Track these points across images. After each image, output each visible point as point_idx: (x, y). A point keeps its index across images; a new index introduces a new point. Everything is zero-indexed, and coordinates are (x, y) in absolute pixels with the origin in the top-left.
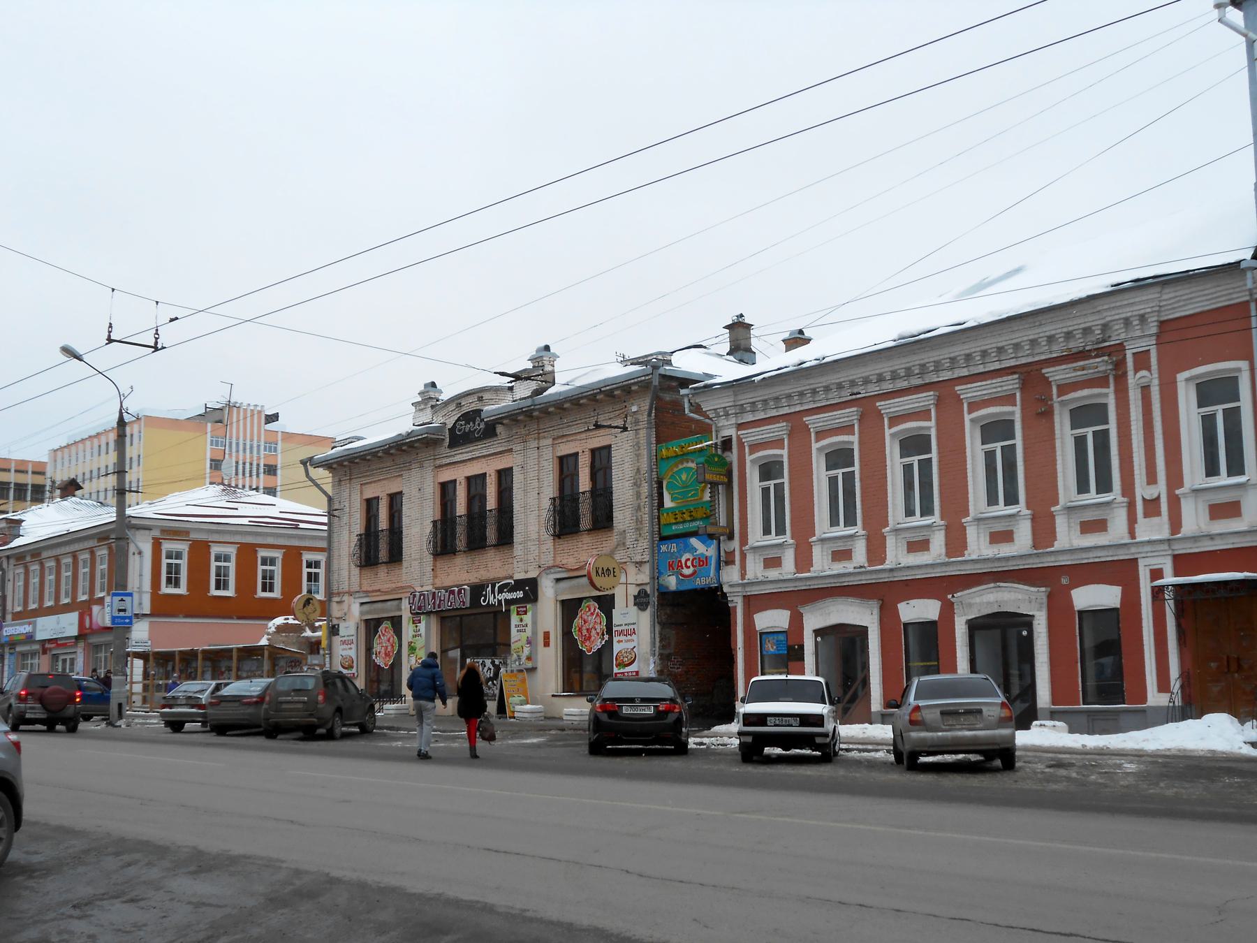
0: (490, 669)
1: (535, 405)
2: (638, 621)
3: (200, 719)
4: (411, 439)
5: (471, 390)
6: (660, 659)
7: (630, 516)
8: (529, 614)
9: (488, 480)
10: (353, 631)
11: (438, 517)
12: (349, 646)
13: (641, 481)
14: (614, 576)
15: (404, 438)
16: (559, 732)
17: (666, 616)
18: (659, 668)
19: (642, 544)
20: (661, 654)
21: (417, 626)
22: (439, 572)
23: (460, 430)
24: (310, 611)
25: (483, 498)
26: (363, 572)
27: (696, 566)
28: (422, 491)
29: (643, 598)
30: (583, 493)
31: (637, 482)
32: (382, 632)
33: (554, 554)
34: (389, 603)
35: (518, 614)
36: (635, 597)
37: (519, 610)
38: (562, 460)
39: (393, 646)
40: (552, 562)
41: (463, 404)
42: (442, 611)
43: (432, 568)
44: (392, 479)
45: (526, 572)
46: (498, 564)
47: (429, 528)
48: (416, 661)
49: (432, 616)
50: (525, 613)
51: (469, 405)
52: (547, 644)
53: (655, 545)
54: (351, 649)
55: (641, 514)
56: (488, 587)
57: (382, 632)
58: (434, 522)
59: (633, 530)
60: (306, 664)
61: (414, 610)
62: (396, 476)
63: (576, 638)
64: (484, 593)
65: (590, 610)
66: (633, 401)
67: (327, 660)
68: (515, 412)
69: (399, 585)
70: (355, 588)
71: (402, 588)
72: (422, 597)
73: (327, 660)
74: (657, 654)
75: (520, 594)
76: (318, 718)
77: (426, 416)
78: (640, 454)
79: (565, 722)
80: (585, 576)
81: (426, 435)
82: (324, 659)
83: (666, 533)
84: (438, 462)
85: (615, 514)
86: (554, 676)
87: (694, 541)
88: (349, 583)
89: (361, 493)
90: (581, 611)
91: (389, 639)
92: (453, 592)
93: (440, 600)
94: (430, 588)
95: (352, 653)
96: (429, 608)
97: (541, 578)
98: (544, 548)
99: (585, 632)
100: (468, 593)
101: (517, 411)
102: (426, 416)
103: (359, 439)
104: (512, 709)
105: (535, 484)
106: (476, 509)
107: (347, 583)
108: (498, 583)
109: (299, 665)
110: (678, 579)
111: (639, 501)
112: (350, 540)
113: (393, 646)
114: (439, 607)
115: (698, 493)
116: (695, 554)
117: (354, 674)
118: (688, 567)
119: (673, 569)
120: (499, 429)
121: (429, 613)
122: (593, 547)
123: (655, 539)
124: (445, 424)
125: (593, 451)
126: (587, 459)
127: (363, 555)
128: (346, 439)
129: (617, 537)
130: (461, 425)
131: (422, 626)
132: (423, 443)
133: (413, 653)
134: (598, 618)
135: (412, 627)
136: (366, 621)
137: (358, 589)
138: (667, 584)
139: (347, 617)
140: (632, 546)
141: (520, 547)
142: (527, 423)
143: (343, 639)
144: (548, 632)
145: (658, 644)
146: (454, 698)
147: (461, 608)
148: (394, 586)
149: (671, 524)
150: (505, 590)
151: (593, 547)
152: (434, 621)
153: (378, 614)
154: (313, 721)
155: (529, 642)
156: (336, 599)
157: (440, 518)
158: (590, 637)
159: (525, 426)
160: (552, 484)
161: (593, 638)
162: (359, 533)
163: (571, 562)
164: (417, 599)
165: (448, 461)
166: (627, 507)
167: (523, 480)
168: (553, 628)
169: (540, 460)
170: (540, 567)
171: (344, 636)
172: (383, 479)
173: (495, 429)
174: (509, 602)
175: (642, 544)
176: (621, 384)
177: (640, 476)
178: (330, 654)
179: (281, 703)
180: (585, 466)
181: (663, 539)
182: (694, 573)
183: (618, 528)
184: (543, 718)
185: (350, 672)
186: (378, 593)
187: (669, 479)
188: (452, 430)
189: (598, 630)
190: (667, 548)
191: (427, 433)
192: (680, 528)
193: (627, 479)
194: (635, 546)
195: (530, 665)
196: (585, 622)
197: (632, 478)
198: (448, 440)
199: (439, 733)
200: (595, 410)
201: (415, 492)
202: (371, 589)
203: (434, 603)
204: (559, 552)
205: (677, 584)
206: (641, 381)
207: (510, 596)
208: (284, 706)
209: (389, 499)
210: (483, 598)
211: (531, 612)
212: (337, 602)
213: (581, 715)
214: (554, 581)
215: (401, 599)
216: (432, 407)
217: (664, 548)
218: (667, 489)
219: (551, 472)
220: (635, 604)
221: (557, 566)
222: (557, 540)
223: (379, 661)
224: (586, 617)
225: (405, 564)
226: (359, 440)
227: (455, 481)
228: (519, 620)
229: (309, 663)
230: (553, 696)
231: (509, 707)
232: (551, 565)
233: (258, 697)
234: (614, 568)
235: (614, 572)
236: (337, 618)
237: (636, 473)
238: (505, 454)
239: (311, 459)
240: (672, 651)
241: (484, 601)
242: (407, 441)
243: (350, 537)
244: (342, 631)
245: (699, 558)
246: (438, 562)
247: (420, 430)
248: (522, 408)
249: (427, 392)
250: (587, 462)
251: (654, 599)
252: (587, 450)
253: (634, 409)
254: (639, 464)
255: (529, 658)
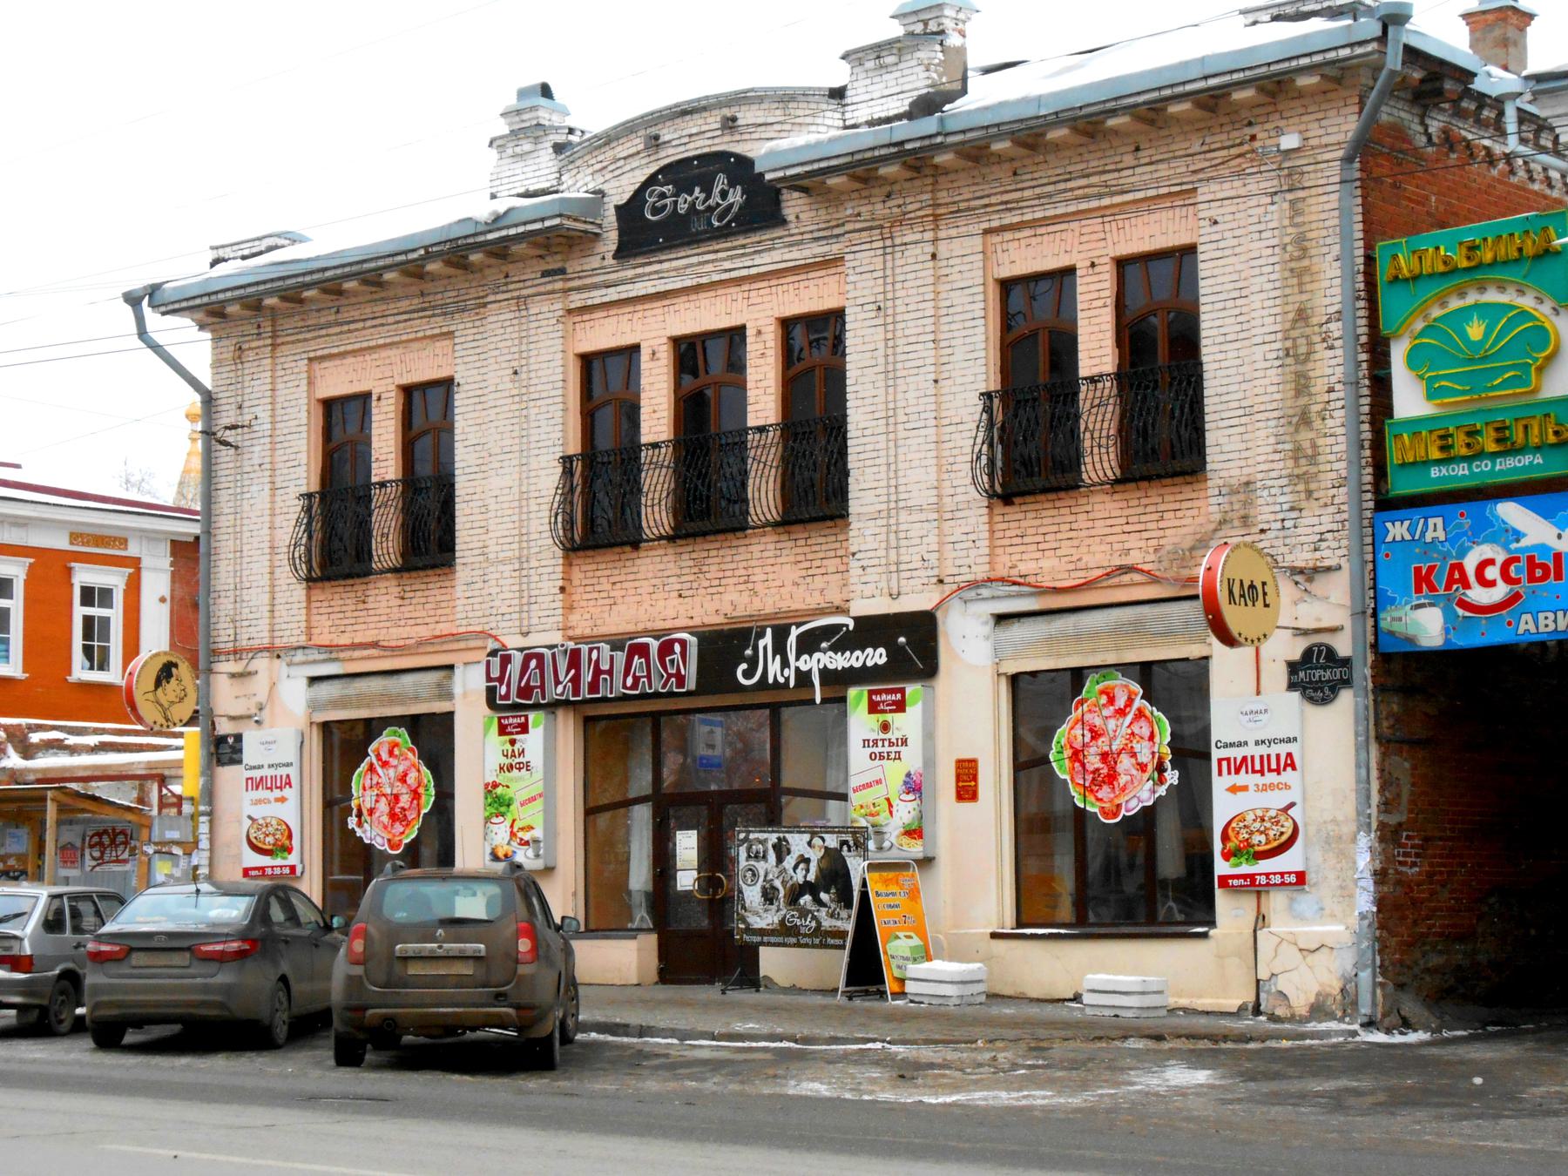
0: (807, 861)
1: (947, 135)
2: (1303, 729)
3: (17, 999)
4: (504, 233)
5: (699, 100)
6: (1381, 839)
7: (1272, 440)
8: (914, 711)
9: (753, 346)
10: (291, 755)
11: (575, 447)
12: (277, 793)
13: (1310, 344)
14: (1266, 606)
15: (480, 228)
16: (1151, 1044)
17: (1392, 721)
18: (1378, 866)
19: (1316, 520)
20: (1382, 826)
21: (513, 742)
22: (578, 595)
23: (655, 211)
24: (172, 696)
25: (631, 412)
26: (317, 595)
27: (1518, 581)
28: (524, 376)
29: (1324, 668)
30: (1093, 380)
31: (1295, 347)
32: (379, 757)
33: (992, 547)
34: (408, 679)
35: (873, 708)
36: (1293, 667)
37: (877, 698)
38: (331, 408)
39: (416, 795)
40: (987, 567)
41: (667, 138)
42: (605, 700)
43: (560, 583)
44: (415, 345)
45: (895, 596)
46: (789, 573)
47: (549, 479)
48: (513, 834)
49: (560, 713)
50: (900, 707)
51: (696, 140)
52: (967, 790)
53: (1366, 523)
54: (283, 800)
55: (1311, 435)
56: (761, 635)
57: (379, 757)
58: (567, 461)
59: (1284, 481)
60: (150, 842)
61: (507, 697)
62: (433, 337)
63: (1063, 776)
64: (749, 652)
65: (1111, 700)
66: (1282, 123)
67: (204, 828)
68: (877, 153)
69: (444, 628)
70: (292, 634)
71: (455, 638)
72: (533, 663)
73: (204, 828)
74: (1374, 825)
75: (877, 657)
76: (518, 1007)
77: (540, 169)
78: (1307, 269)
79: (1089, 1011)
80: (1195, 597)
81: (557, 221)
82: (195, 828)
83: (1401, 485)
84: (577, 300)
85: (1210, 438)
86: (993, 883)
87: (1510, 512)
88: (272, 625)
89: (311, 383)
90: (1082, 702)
91: (406, 775)
92: (643, 650)
93: (598, 672)
94: (556, 638)
95: (288, 813)
96: (556, 692)
97: (947, 611)
98: (956, 531)
99: (1094, 761)
100: (693, 652)
101: (883, 152)
102: (540, 169)
103: (294, 239)
104: (897, 973)
105: (927, 353)
106: (604, 442)
107: (264, 625)
108: (798, 625)
109: (126, 843)
110: (1448, 615)
111: (1303, 401)
112: (273, 509)
113: (416, 795)
114: (594, 687)
115: (1528, 374)
116: (1514, 546)
117: (293, 868)
118: (1489, 584)
119: (1432, 588)
120: (793, 205)
121: (553, 706)
122: (1127, 528)
123: (1365, 505)
124: (601, 193)
125: (408, 391)
126: (1107, 293)
127: (315, 551)
128: (259, 239)
129: (1221, 499)
130: (663, 196)
131: (533, 743)
132: (536, 245)
133: (503, 815)
134: (1143, 722)
135: (496, 744)
136: (326, 727)
137: (303, 640)
138: (1411, 631)
139: (265, 714)
140: (1279, 525)
141: (871, 528)
142: (896, 187)
143: (256, 774)
144: (974, 762)
145: (1375, 798)
146: (642, 937)
147: (671, 694)
148: (424, 632)
149: (1427, 463)
150: (824, 645)
151: (1127, 528)
152: (567, 730)
153: (368, 706)
154: (507, 1014)
155: (913, 787)
156: (227, 666)
157: (579, 451)
158: (1112, 777)
159: (889, 196)
160: (983, 354)
161: (1123, 779)
162: (304, 490)
163: (1051, 567)
164: (514, 668)
165: (613, 294)
166: (1259, 417)
167: (881, 345)
168: (990, 747)
169: (941, 288)
170: (941, 581)
171: (260, 767)
172: (385, 346)
173: (777, 203)
174: (837, 681)
175: (1316, 520)
176: (1264, 69)
177: (1308, 331)
178: (210, 814)
179: (405, 959)
180: (1100, 303)
181: (1386, 504)
182: (1514, 599)
183: (1223, 474)
184: (983, 998)
185: (278, 861)
186: (374, 652)
187: (1422, 334)
188: (629, 212)
189: (1144, 757)
190: (1411, 530)
191: (560, 215)
192: (1460, 474)
193: (1258, 340)
194: (1288, 524)
195: (916, 849)
196: (1096, 734)
197: (1280, 336)
198: (613, 236)
199: (792, 1045)
200: (1137, 149)
201: (498, 377)
202: (348, 642)
203: (576, 681)
204: (1007, 542)
205: (1447, 631)
206: (1333, 62)
207: (839, 661)
208: (414, 970)
209: (401, 401)
210: (744, 666)
211: (919, 705)
212: (233, 676)
213: (1143, 993)
214: (992, 622)
215: (451, 667)
216: (559, 148)
217: (1397, 530)
218: (1412, 361)
219: (305, 428)
220: (1292, 686)
221: (1002, 580)
222: (999, 508)
223: (373, 834)
224: (1098, 722)
225: (462, 573)
226: (294, 242)
227: (635, 349)
228: (876, 726)
229: (155, 838)
230: (994, 936)
231: (889, 965)
232: (980, 577)
233: (243, 935)
234: (1264, 584)
235: (1265, 594)
236: (233, 718)
237: (1295, 321)
238: (811, 275)
239: (153, 290)
240: (1404, 818)
241: (748, 674)
242: (490, 237)
243: (273, 502)
244: (252, 751)
245: (1531, 559)
246: (575, 569)
247: (535, 206)
248: (902, 143)
249: (533, 108)
250: (1103, 294)
251: (1363, 672)
252: (1106, 260)
253: (1289, 141)
254: (1304, 297)
255: (914, 833)
